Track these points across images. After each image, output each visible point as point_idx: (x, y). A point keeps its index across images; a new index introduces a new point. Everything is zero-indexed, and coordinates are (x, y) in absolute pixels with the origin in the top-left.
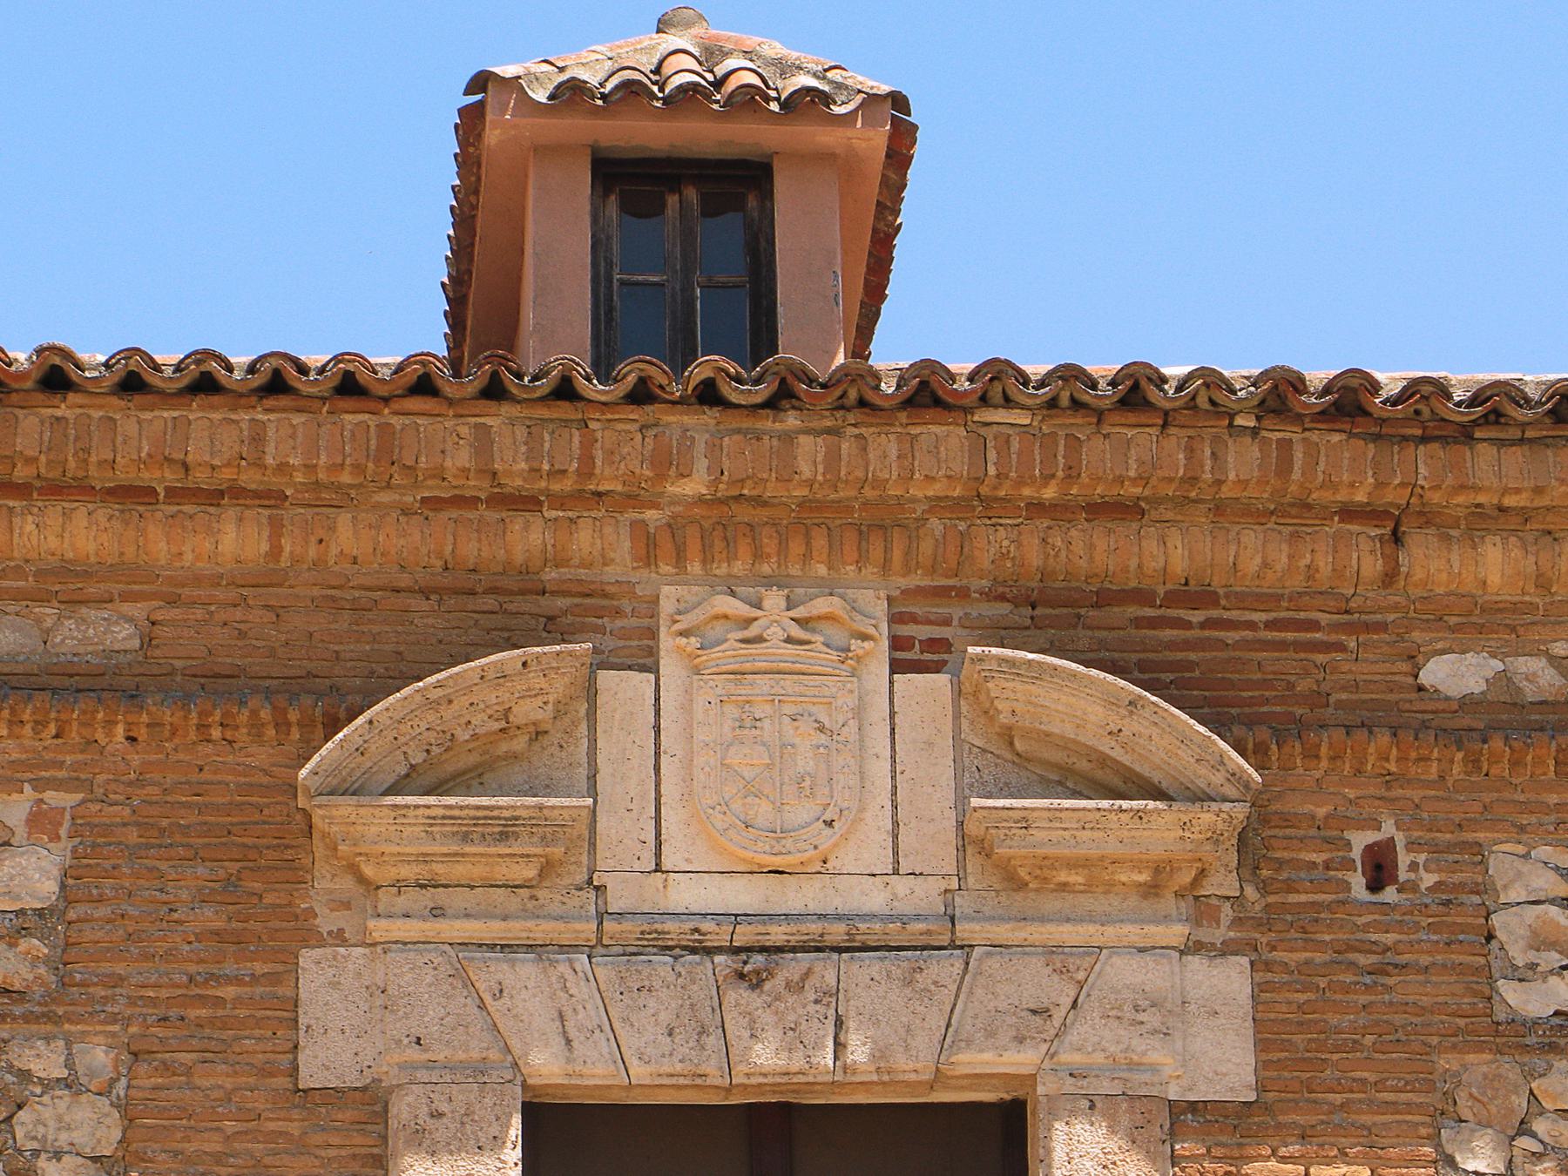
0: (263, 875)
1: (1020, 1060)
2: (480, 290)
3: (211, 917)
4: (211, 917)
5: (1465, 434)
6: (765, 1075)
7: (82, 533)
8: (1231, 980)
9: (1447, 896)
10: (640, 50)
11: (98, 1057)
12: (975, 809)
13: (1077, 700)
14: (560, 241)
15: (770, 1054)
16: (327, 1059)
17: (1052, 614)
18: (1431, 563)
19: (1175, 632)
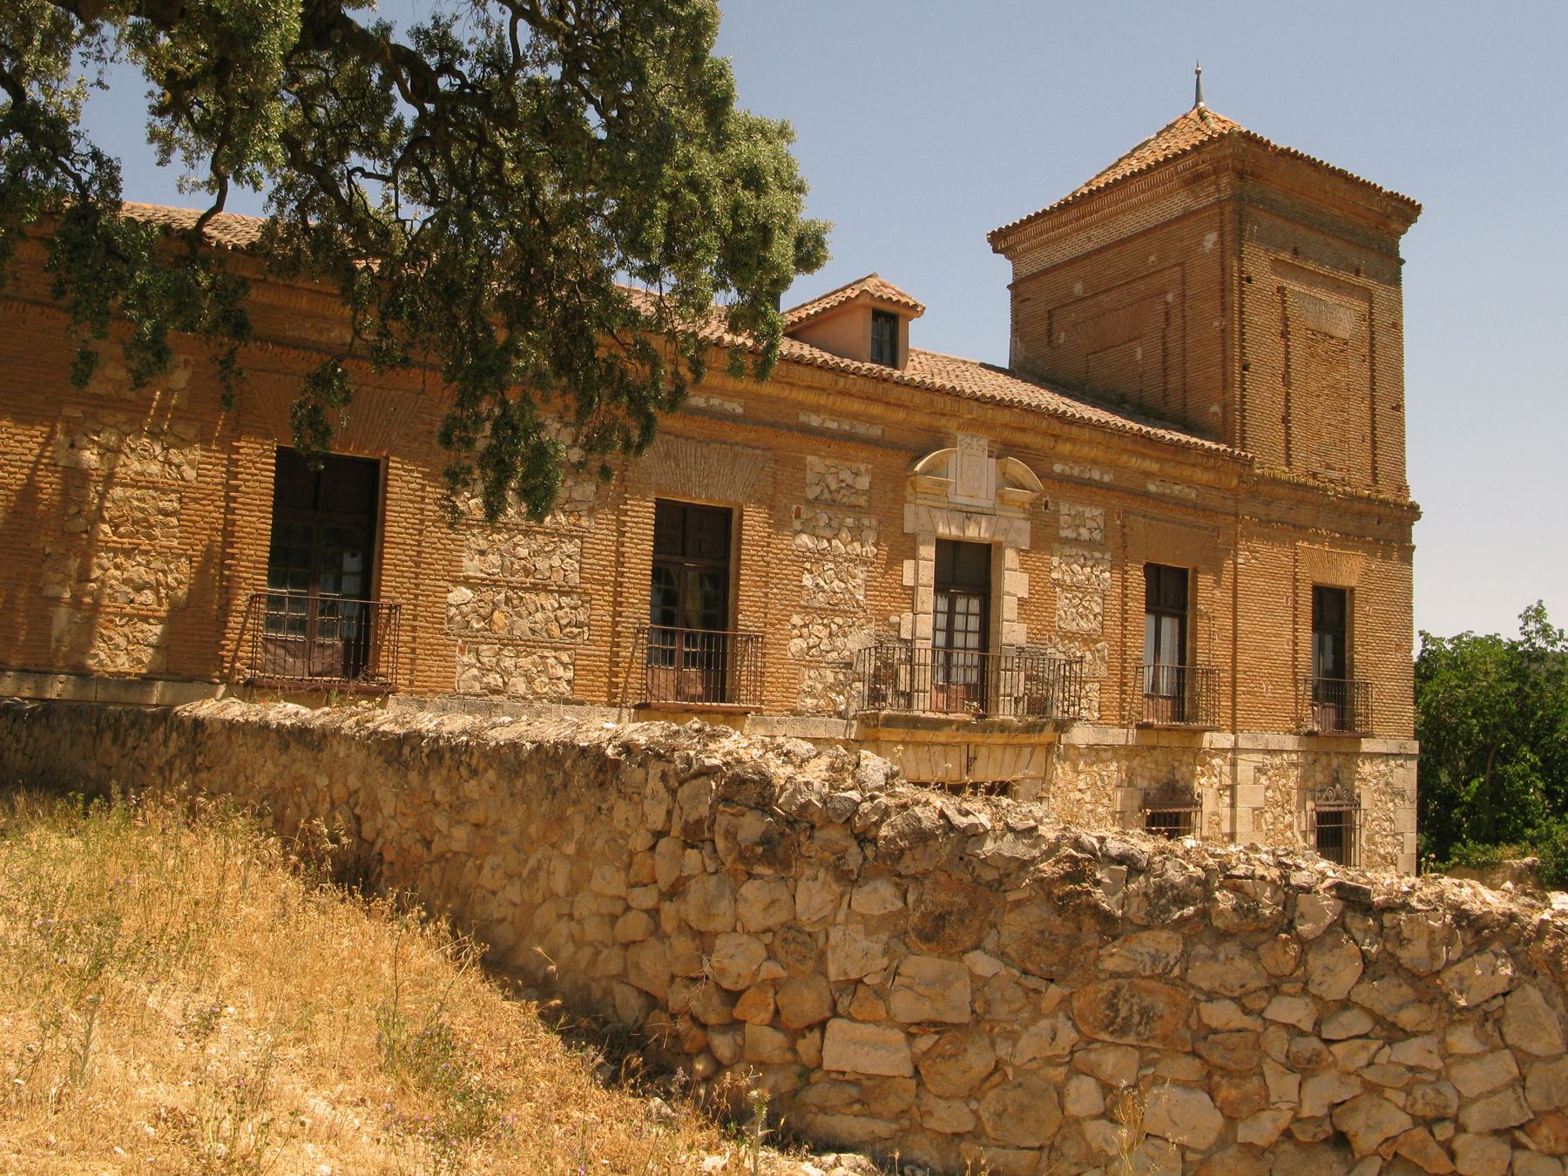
3: (891, 495)
4: (891, 495)
8: (1027, 526)
11: (874, 522)
12: (785, 359)
13: (1017, 467)
16: (908, 528)
19: (817, 353)
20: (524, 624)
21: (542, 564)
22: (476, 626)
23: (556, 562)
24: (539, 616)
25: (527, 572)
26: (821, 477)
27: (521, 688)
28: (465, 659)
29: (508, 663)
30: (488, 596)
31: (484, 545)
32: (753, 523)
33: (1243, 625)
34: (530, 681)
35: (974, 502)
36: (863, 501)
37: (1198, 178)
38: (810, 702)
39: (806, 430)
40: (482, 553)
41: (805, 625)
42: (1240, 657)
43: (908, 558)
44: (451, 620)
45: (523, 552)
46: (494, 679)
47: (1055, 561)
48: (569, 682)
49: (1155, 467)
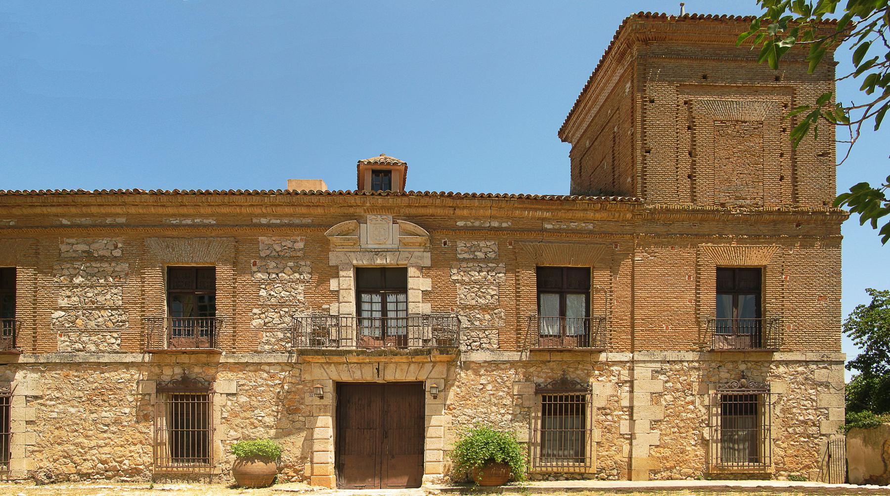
0: (325, 245)
1: (406, 262)
2: (360, 184)
5: (463, 198)
6: (89, 256)
7: (304, 210)
8: (429, 254)
9: (452, 246)
10: (378, 158)
13: (410, 226)
14: (368, 178)
15: (379, 262)
17: (410, 218)
18: (458, 212)
20: (93, 323)
21: (99, 298)
22: (67, 325)
23: (108, 297)
24: (100, 319)
25: (93, 303)
26: (269, 247)
27: (93, 348)
28: (63, 339)
29: (84, 339)
30: (73, 313)
31: (70, 294)
32: (223, 273)
33: (638, 293)
34: (97, 345)
35: (382, 246)
36: (299, 254)
37: (622, 55)
38: (266, 347)
39: (261, 225)
40: (69, 297)
41: (263, 313)
42: (637, 311)
43: (333, 277)
44: (54, 324)
45: (89, 295)
46: (79, 346)
47: (455, 271)
48: (118, 345)
49: (547, 215)
